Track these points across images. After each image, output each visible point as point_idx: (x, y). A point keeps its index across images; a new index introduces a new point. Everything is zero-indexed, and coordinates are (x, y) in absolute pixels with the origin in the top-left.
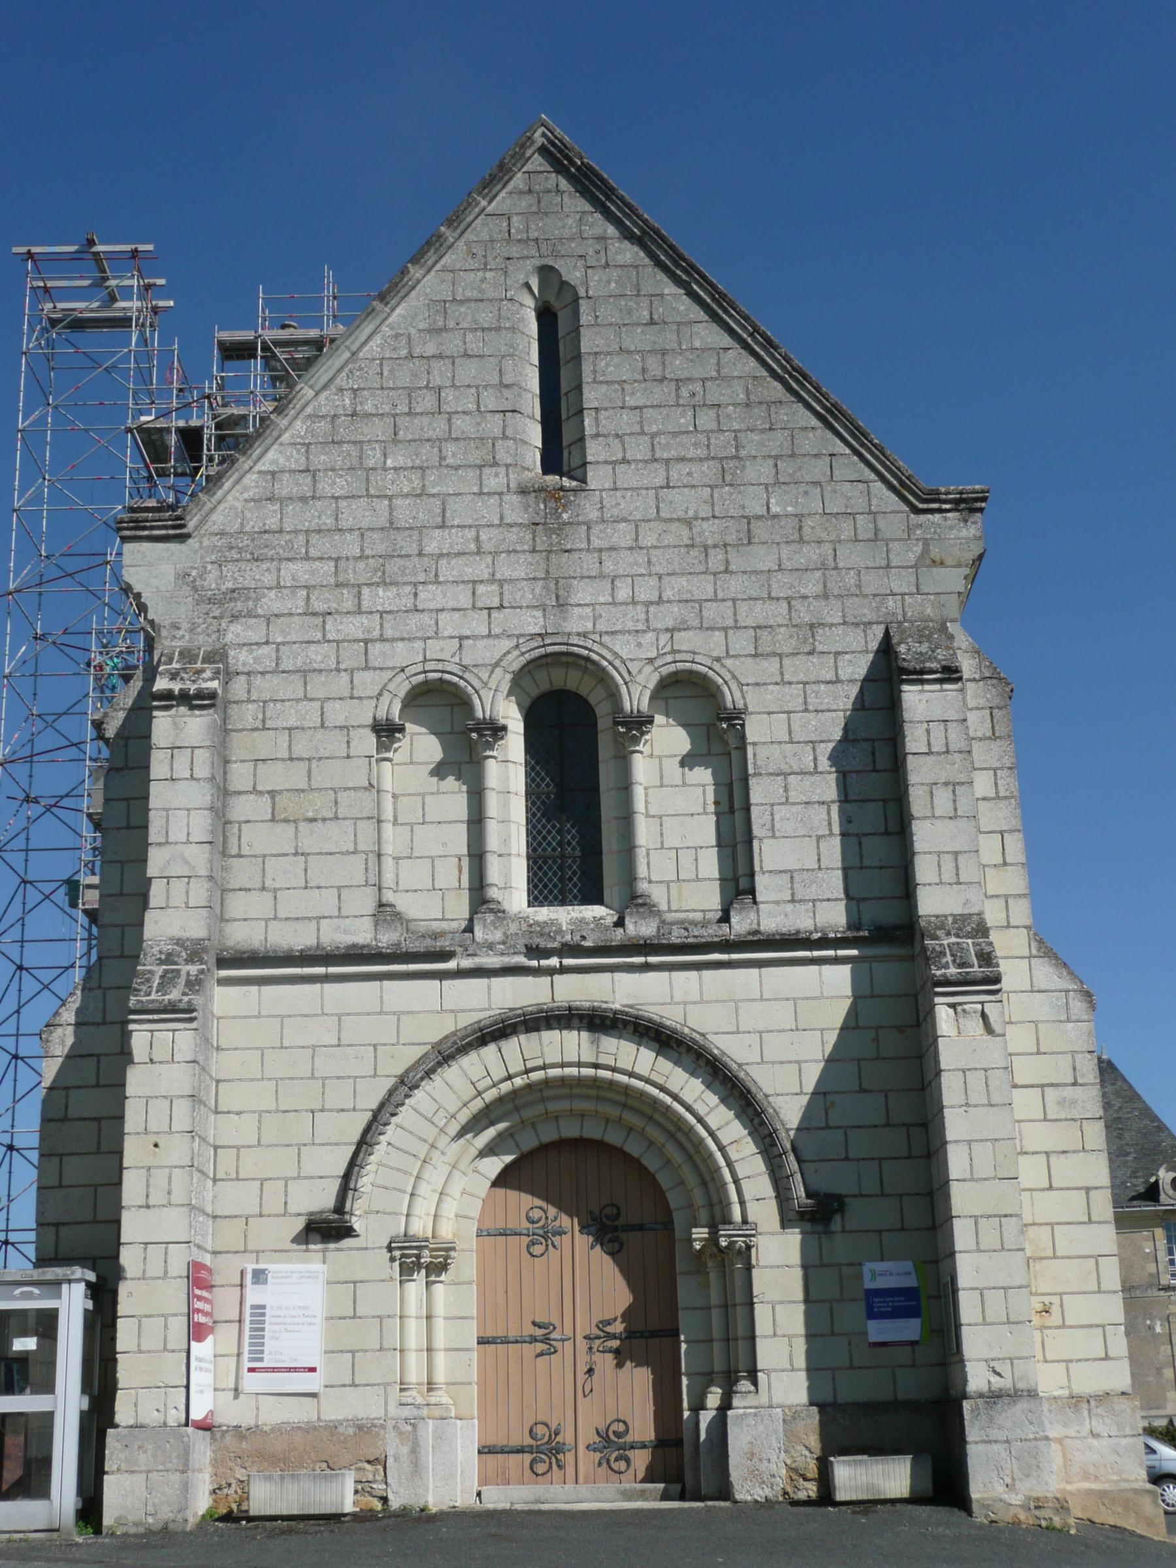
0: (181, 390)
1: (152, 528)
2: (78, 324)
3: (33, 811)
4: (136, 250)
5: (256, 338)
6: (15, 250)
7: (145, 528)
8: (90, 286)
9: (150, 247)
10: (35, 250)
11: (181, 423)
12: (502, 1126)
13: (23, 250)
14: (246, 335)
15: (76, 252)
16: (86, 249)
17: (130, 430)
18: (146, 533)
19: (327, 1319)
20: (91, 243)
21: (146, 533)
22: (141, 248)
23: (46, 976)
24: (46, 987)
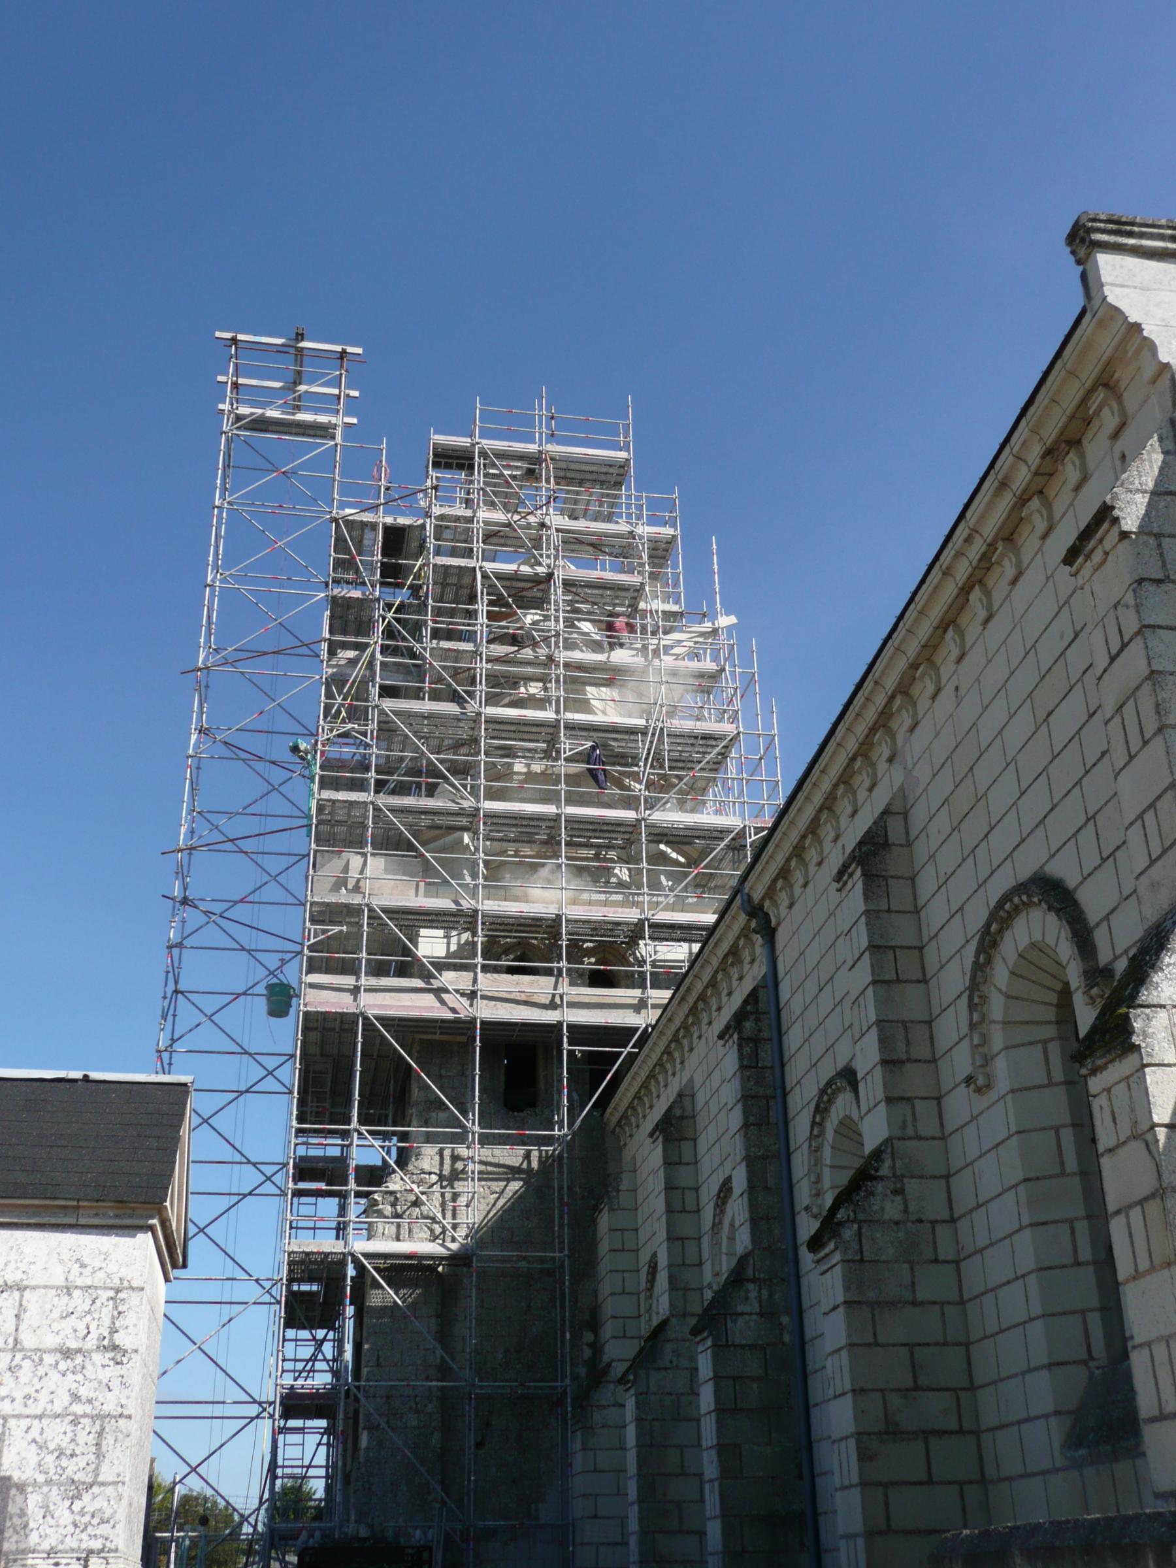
0: (388, 489)
1: (1142, 235)
2: (261, 425)
3: (193, 917)
4: (344, 352)
5: (473, 445)
6: (218, 334)
7: (1130, 234)
8: (281, 388)
9: (359, 351)
10: (240, 337)
11: (389, 520)
12: (158, 1535)
13: (228, 335)
14: (463, 441)
15: (282, 345)
16: (292, 343)
17: (336, 520)
18: (1132, 241)
19: (822, 1335)
20: (300, 337)
21: (1132, 241)
22: (350, 350)
23: (271, 1063)
24: (270, 1073)
